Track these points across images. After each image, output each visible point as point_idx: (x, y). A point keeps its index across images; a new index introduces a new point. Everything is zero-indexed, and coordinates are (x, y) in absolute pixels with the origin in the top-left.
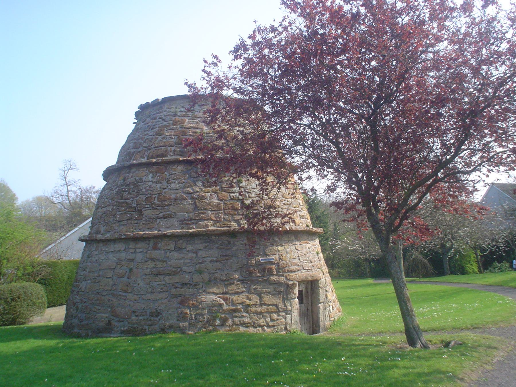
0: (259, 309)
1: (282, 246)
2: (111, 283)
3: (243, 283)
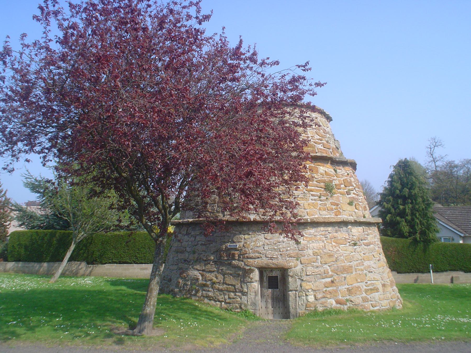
0: (221, 287)
1: (249, 235)
3: (216, 264)
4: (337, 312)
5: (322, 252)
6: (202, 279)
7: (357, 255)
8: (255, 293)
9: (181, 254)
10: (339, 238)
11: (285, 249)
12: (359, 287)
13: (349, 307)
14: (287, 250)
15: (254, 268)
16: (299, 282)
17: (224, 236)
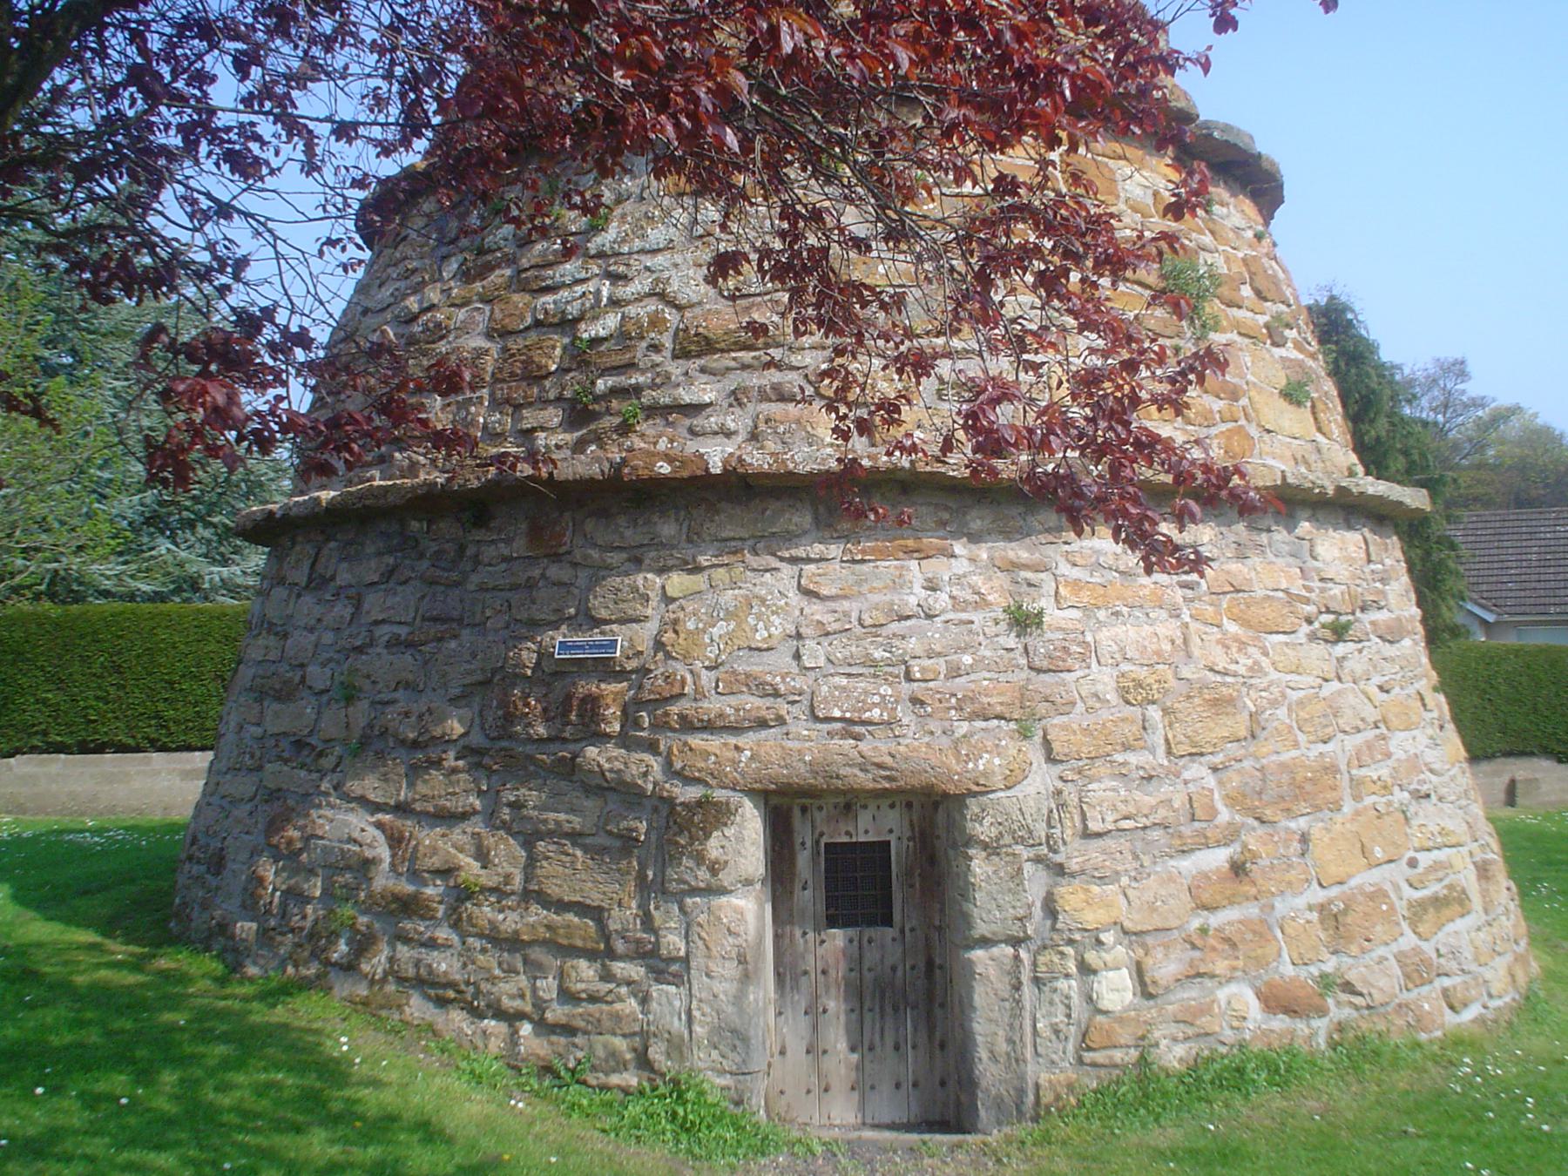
0: (509, 921)
1: (698, 569)
3: (479, 765)
4: (1282, 1068)
5: (1172, 683)
6: (393, 864)
7: (1352, 699)
8: (742, 960)
9: (276, 706)
10: (1260, 593)
11: (941, 665)
12: (1378, 895)
13: (1341, 1027)
14: (955, 672)
15: (735, 797)
16: (1036, 883)
17: (530, 585)
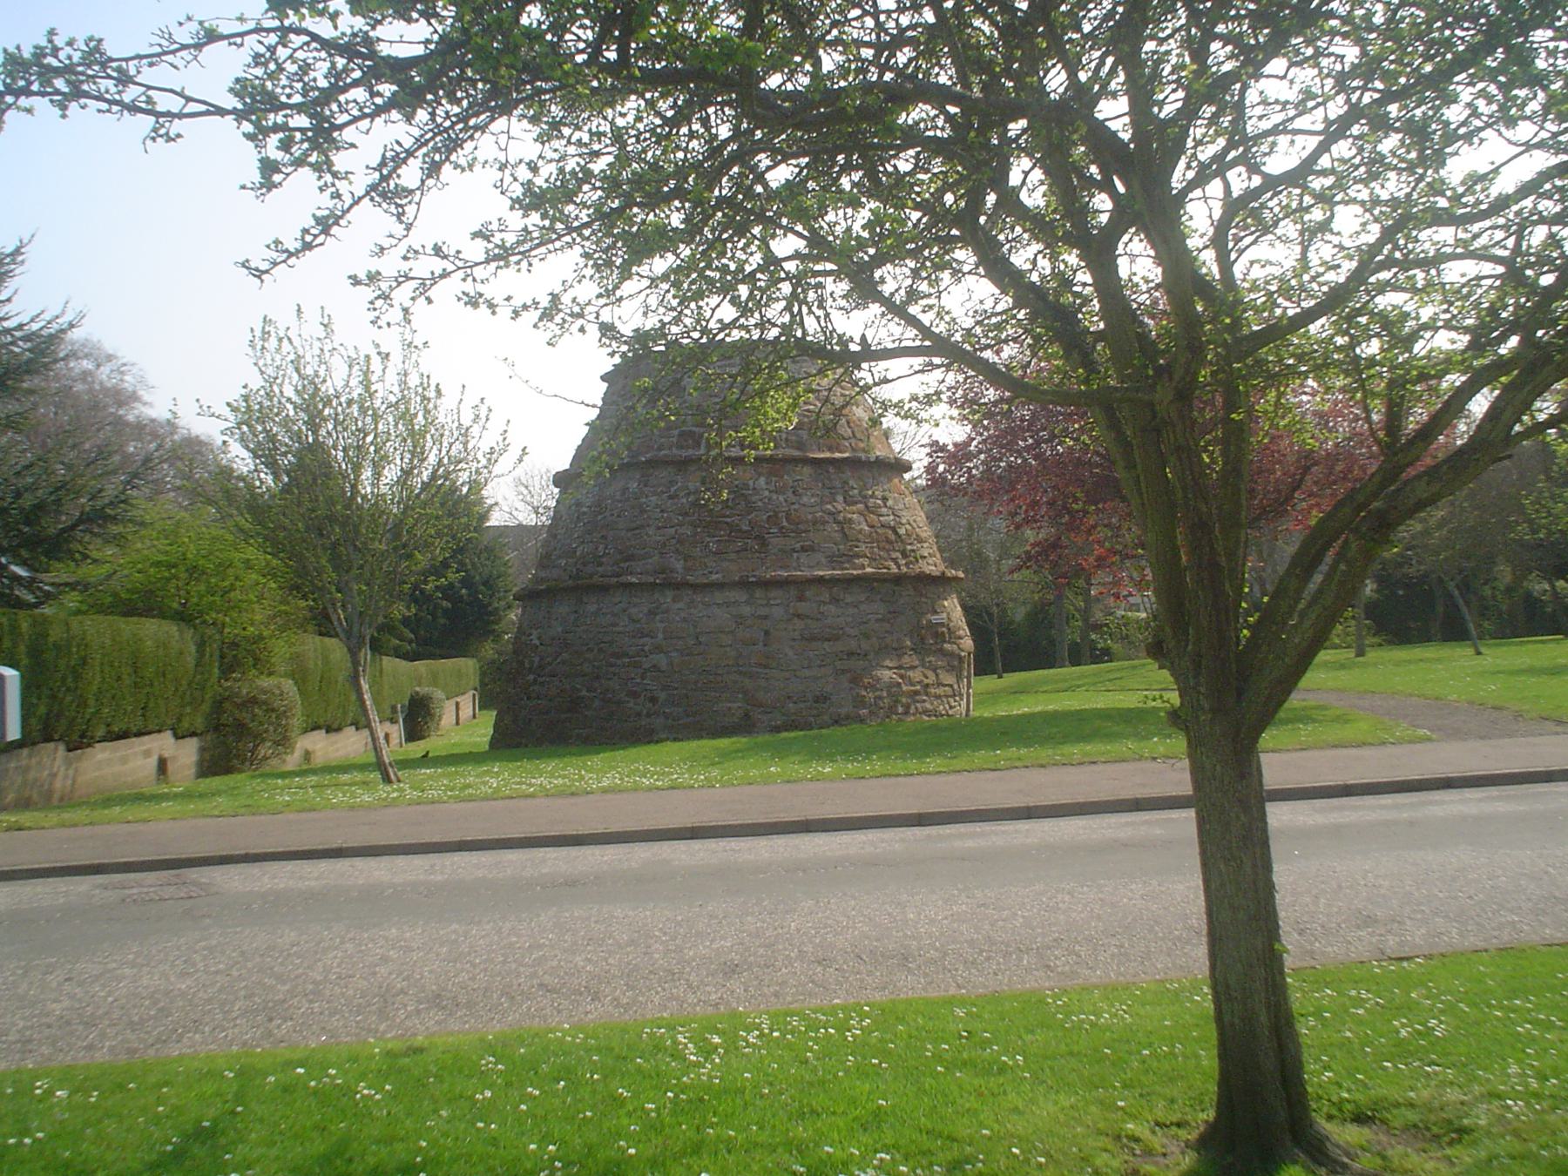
2: (733, 653)
